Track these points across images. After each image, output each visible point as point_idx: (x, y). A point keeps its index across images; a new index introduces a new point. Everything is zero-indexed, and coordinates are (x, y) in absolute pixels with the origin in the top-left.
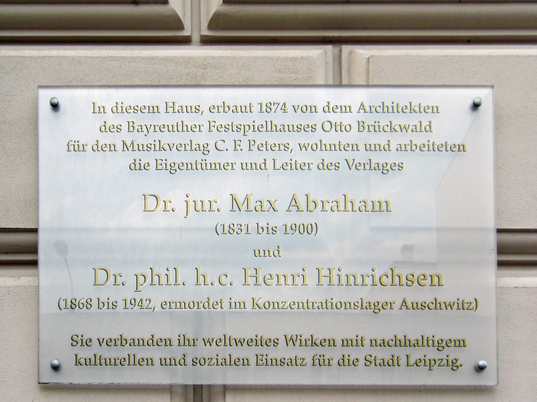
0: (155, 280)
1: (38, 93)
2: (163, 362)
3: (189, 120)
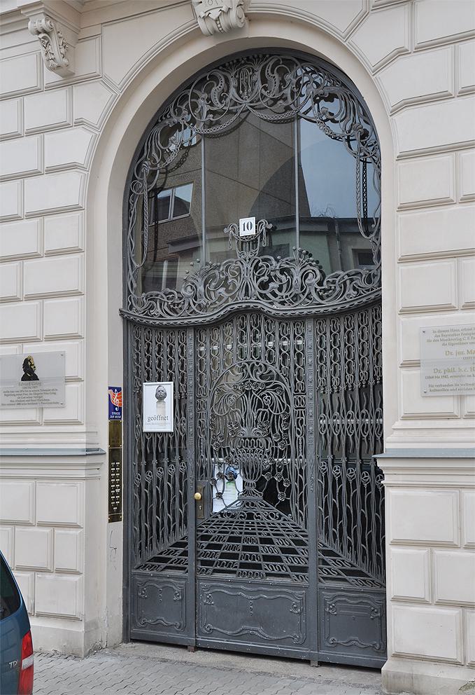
0: (449, 371)
1: (141, 388)
2: (451, 390)
3: (456, 333)
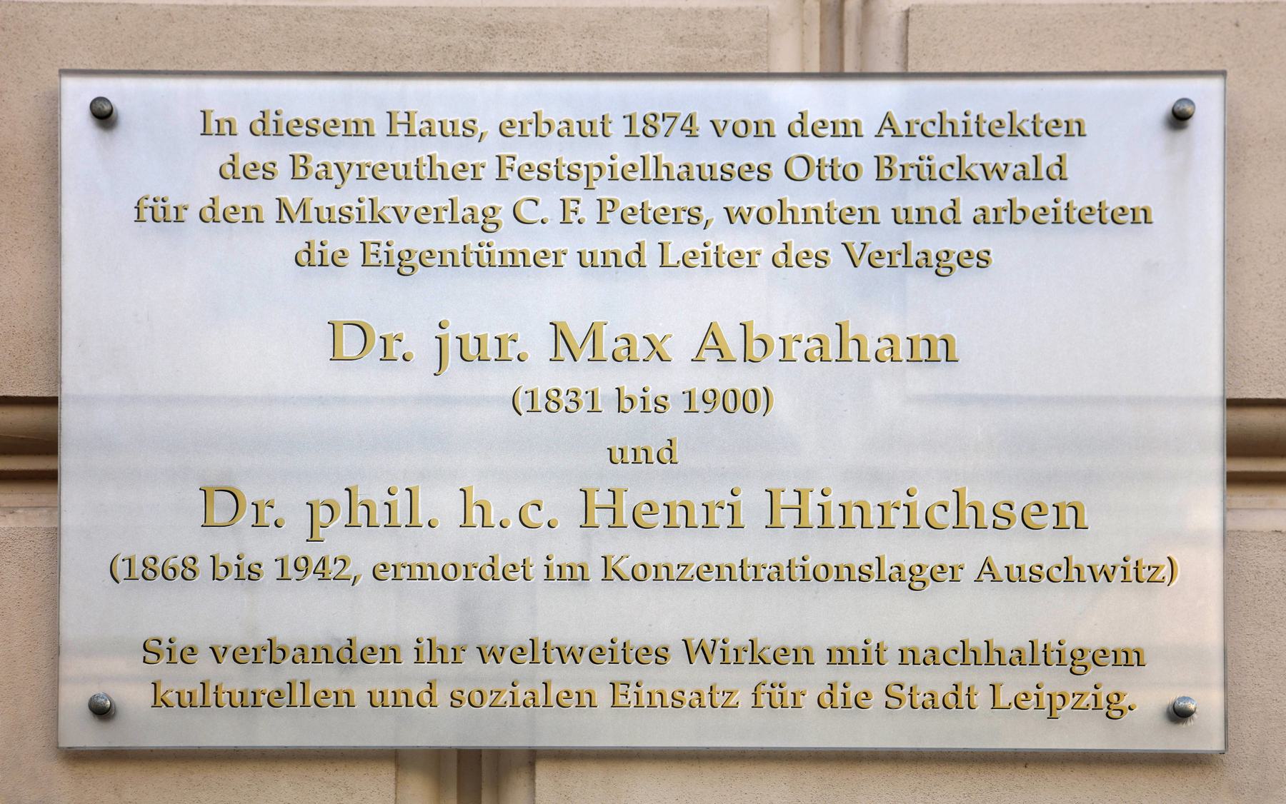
0: (357, 512)
3: (449, 153)
